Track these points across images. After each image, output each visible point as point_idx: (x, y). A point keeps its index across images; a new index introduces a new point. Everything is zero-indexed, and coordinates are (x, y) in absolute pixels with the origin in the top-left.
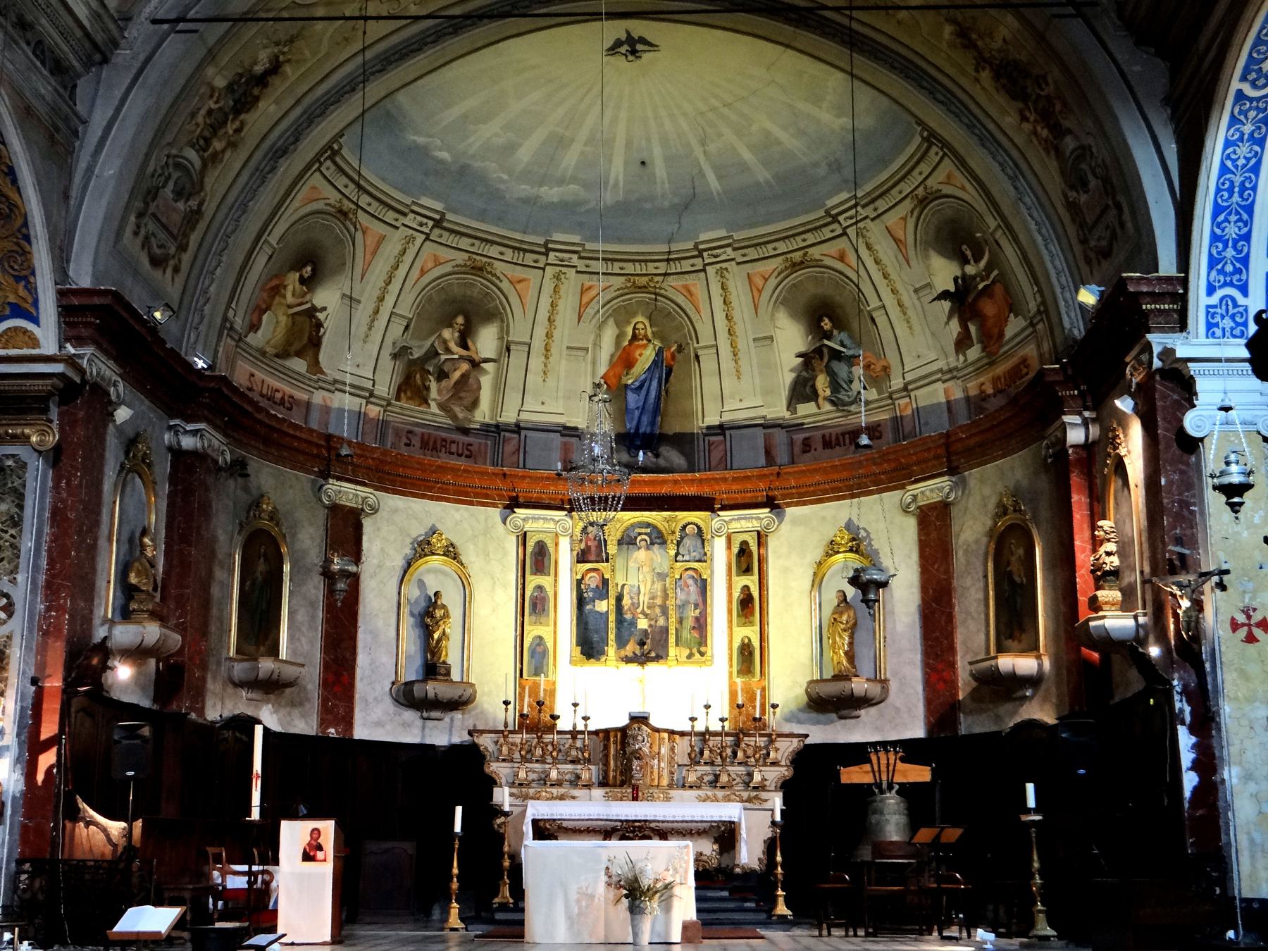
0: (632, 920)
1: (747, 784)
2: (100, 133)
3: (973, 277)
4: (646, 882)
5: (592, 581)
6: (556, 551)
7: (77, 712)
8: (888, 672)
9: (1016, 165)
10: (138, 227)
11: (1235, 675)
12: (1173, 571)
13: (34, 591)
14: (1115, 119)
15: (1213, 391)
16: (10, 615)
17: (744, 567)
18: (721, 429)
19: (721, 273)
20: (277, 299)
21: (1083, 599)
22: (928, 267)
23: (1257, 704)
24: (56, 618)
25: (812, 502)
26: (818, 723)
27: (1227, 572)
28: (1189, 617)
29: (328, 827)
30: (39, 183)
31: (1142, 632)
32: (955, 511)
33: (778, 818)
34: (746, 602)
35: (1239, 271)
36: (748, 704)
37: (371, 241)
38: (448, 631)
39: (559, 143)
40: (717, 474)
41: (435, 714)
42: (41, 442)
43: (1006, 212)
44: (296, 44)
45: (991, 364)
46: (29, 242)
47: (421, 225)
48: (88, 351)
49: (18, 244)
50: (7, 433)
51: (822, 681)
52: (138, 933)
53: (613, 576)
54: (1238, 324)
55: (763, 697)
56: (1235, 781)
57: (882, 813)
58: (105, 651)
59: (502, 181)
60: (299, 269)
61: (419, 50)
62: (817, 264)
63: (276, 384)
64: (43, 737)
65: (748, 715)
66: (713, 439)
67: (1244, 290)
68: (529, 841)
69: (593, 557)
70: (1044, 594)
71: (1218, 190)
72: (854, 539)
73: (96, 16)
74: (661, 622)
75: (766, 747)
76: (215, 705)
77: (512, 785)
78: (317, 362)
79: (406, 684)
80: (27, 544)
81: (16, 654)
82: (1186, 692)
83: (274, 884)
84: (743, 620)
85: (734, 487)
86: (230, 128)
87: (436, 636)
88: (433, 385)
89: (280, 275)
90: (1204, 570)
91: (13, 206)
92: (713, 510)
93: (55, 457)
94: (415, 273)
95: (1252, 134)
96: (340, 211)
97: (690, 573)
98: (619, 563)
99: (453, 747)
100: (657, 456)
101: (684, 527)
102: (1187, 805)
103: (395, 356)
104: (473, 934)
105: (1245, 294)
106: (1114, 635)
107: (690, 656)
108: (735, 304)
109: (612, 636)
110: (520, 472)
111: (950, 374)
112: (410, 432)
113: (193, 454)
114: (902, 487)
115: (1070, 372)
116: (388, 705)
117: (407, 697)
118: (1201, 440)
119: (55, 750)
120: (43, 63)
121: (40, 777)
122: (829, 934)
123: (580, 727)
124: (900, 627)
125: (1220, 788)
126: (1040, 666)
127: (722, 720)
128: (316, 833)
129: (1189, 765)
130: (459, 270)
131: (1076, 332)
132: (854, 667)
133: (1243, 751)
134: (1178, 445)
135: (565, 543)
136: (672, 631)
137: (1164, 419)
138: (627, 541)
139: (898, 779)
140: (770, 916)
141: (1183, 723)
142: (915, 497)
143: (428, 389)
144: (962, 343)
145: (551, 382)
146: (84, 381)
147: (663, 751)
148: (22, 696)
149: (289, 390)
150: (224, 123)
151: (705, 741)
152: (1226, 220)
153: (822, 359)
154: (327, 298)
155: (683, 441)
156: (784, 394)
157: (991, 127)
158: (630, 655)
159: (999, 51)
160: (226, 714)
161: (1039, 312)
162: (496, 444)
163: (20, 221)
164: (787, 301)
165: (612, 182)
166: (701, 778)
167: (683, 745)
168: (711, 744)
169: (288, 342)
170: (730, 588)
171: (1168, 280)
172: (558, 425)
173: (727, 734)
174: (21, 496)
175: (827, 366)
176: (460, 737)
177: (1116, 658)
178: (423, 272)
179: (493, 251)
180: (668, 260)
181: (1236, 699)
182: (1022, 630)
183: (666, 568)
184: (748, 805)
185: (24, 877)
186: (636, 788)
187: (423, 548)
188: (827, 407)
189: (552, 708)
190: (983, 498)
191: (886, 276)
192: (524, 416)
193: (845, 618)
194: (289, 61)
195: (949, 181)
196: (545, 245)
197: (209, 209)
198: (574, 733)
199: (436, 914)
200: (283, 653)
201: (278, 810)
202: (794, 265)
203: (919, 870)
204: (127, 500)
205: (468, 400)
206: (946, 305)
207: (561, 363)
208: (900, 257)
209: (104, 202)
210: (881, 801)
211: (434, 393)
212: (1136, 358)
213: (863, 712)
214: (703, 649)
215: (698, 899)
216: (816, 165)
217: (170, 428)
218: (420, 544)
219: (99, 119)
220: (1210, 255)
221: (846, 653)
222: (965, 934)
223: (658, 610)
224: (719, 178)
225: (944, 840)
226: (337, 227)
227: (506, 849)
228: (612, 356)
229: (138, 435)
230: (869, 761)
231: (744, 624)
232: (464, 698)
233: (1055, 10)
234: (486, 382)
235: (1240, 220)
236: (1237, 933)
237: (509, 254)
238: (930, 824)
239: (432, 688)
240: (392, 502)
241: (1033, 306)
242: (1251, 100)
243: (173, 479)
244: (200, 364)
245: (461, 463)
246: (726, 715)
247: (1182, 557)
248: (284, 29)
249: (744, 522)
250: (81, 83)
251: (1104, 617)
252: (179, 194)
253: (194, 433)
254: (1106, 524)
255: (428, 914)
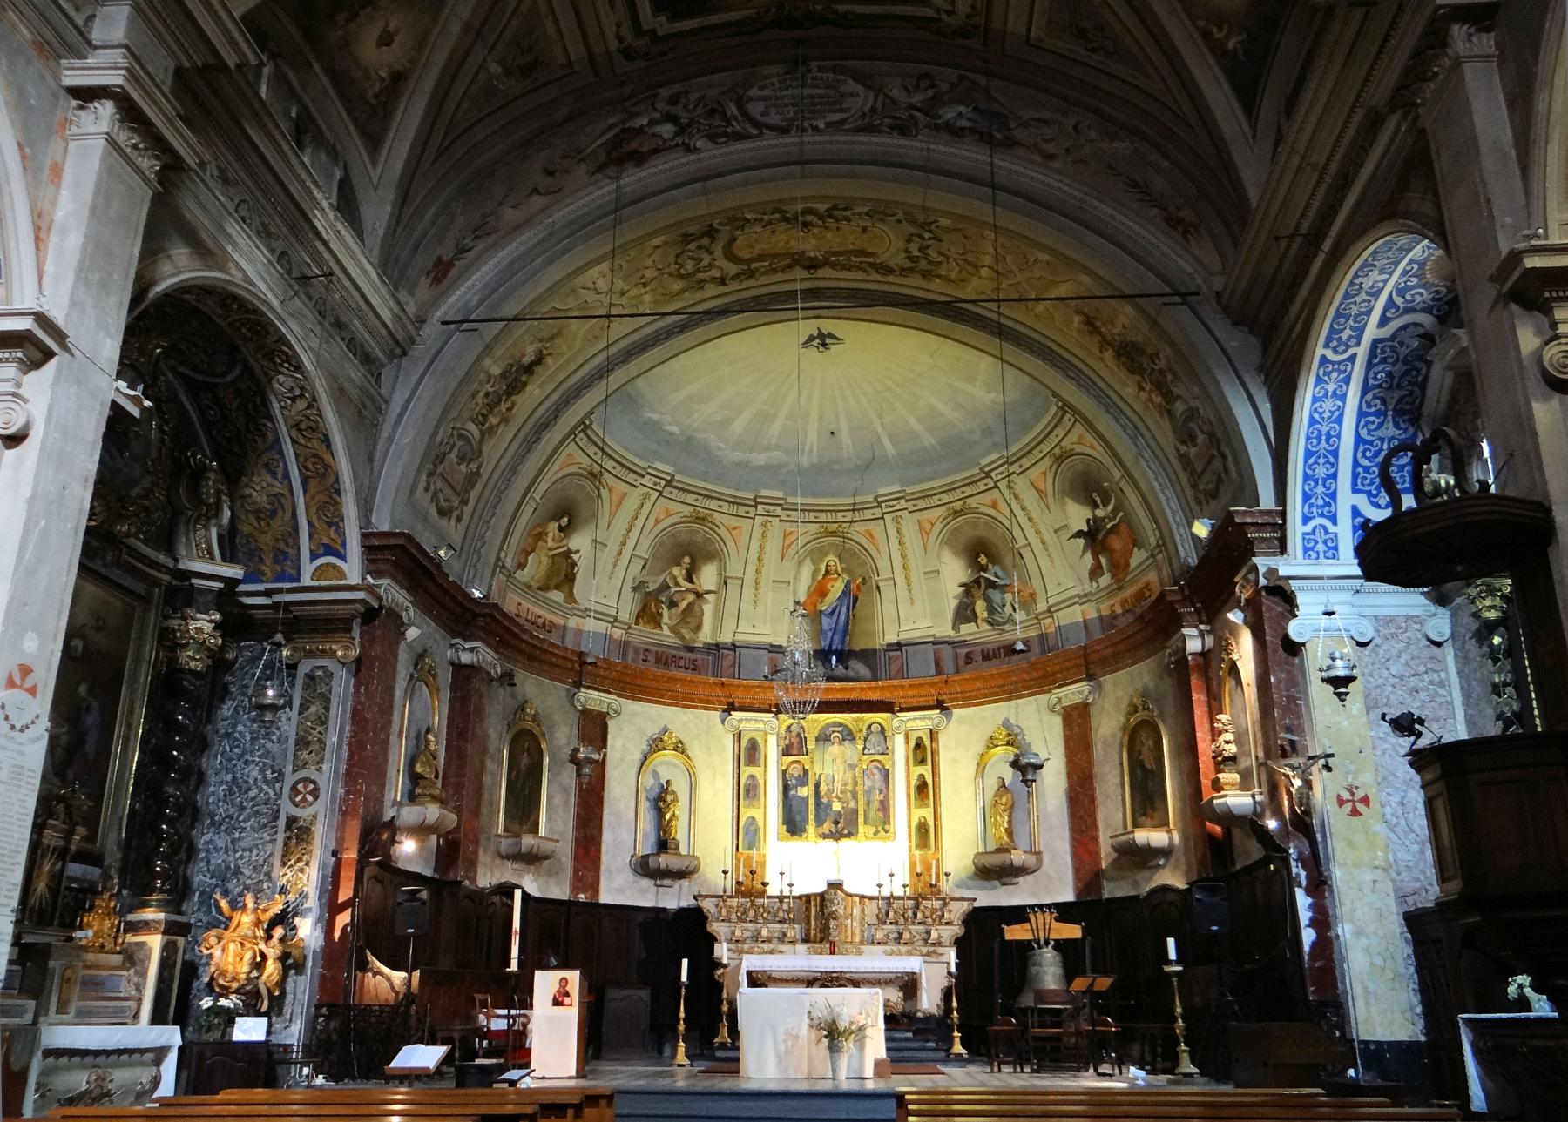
0: (831, 1058)
1: (926, 941)
2: (399, 410)
3: (1103, 519)
4: (843, 1024)
5: (795, 771)
6: (766, 746)
7: (370, 879)
8: (1041, 846)
9: (1136, 427)
10: (429, 484)
11: (1343, 844)
12: (1284, 755)
13: (336, 778)
14: (1217, 383)
15: (1317, 604)
16: (316, 798)
17: (920, 759)
18: (899, 646)
19: (896, 520)
20: (540, 543)
21: (1206, 782)
22: (1064, 512)
23: (1364, 869)
24: (353, 800)
25: (974, 705)
26: (984, 889)
27: (1332, 755)
28: (1301, 794)
29: (574, 976)
30: (348, 449)
31: (1259, 809)
32: (1093, 711)
33: (953, 969)
34: (922, 787)
35: (1329, 505)
36: (925, 873)
37: (615, 498)
38: (677, 812)
39: (766, 417)
40: (896, 682)
41: (666, 882)
42: (344, 656)
43: (1128, 464)
44: (556, 341)
45: (1119, 589)
46: (340, 495)
47: (656, 484)
48: (385, 582)
49: (330, 497)
50: (318, 649)
51: (986, 853)
52: (410, 1068)
53: (813, 768)
54: (1330, 548)
55: (938, 867)
56: (1348, 936)
57: (1040, 965)
58: (392, 827)
59: (719, 448)
60: (558, 520)
61: (653, 346)
62: (974, 511)
63: (539, 612)
64: (340, 900)
65: (925, 883)
66: (891, 654)
67: (1334, 520)
68: (744, 988)
69: (795, 752)
70: (1171, 778)
71: (1308, 438)
72: (1010, 735)
73: (396, 317)
74: (852, 805)
75: (942, 909)
76: (485, 875)
77: (729, 941)
78: (572, 594)
79: (643, 857)
80: (332, 739)
81: (319, 831)
82: (1301, 859)
83: (529, 1026)
84: (920, 803)
85: (910, 693)
86: (503, 407)
87: (667, 817)
88: (665, 612)
89: (542, 524)
90: (1311, 754)
91: (327, 466)
92: (892, 712)
93: (358, 666)
94: (651, 523)
95: (1334, 392)
96: (591, 473)
97: (875, 763)
98: (817, 756)
99: (682, 910)
100: (847, 668)
101: (870, 727)
102: (1306, 958)
103: (635, 589)
104: (697, 1069)
105: (1335, 522)
106: (1235, 811)
107: (876, 833)
108: (908, 544)
109: (811, 817)
110: (736, 681)
111: (1086, 598)
112: (647, 650)
113: (471, 667)
114: (1049, 691)
115: (1187, 593)
116: (628, 874)
117: (645, 868)
118: (1304, 644)
119: (350, 910)
120: (354, 355)
121: (337, 934)
122: (1022, 1072)
123: (786, 893)
124: (1050, 808)
125: (1335, 942)
126: (1171, 839)
127: (904, 886)
128: (564, 980)
129: (1307, 922)
130: (687, 520)
131: (1190, 560)
132: (1012, 841)
133: (1354, 910)
134: (1285, 650)
135: (772, 740)
136: (861, 812)
137: (1270, 628)
138: (824, 738)
139: (1054, 936)
140: (948, 1054)
141: (1300, 886)
142: (1060, 699)
143: (661, 615)
144: (1095, 572)
145: (760, 609)
146: (381, 607)
147: (855, 912)
148: (323, 866)
149: (549, 617)
150: (498, 403)
151: (889, 904)
152: (1316, 462)
153: (979, 587)
154: (580, 542)
155: (868, 656)
156: (950, 617)
157: (1113, 395)
158: (827, 832)
159: (1119, 335)
160: (495, 882)
161: (1158, 545)
162: (716, 660)
163: (332, 479)
164: (951, 541)
165: (807, 447)
166: (887, 936)
167: (872, 909)
168: (895, 906)
169: (548, 577)
170: (908, 776)
171: (1269, 512)
172: (765, 644)
173: (909, 898)
174: (328, 700)
175: (984, 594)
176: (687, 902)
177: (1237, 833)
178: (657, 522)
179: (713, 504)
180: (853, 510)
181: (1346, 864)
182: (1154, 809)
183: (855, 760)
184: (927, 958)
185: (321, 1019)
186: (833, 944)
187: (657, 745)
188: (986, 626)
189: (763, 877)
190: (1117, 698)
191: (1030, 520)
192: (739, 637)
193: (1004, 800)
194: (550, 354)
195: (1080, 442)
196: (755, 499)
197: (486, 472)
198: (781, 898)
199: (667, 1052)
200: (542, 832)
201: (531, 961)
202: (956, 512)
203: (1074, 1015)
204: (414, 703)
205: (693, 623)
206: (1081, 541)
207: (768, 595)
208: (1042, 505)
209: (401, 463)
210: (1040, 954)
211: (666, 619)
212: (1245, 578)
213: (1021, 879)
214: (887, 827)
215: (888, 1040)
216: (972, 432)
217: (452, 646)
218: (654, 741)
219: (398, 399)
220: (1304, 491)
221: (1006, 830)
222: (1117, 1071)
223: (849, 795)
224: (893, 444)
225: (1096, 988)
226: (589, 486)
227: (725, 995)
228: (809, 588)
229: (425, 651)
230: (1028, 920)
231: (921, 806)
232: (691, 868)
233: (1166, 300)
234: (708, 610)
235: (1328, 462)
236: (1357, 1072)
237: (726, 507)
238: (1083, 973)
239: (664, 860)
240: (631, 707)
241: (1153, 541)
242: (1333, 363)
243: (454, 687)
244: (477, 594)
245: (688, 675)
246: (907, 882)
247: (1292, 743)
248: (548, 327)
249: (918, 722)
250: (384, 371)
251: (1225, 796)
252: (462, 458)
253: (471, 650)
254: (1223, 717)
255: (660, 1051)
